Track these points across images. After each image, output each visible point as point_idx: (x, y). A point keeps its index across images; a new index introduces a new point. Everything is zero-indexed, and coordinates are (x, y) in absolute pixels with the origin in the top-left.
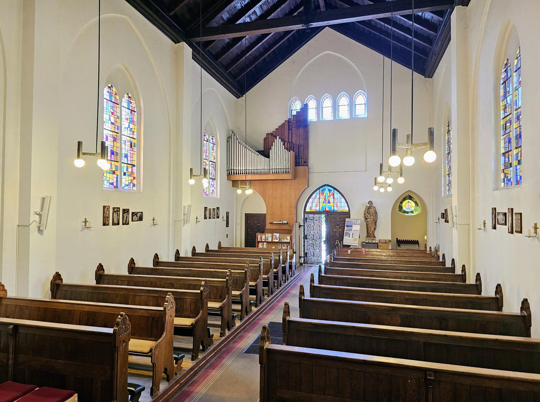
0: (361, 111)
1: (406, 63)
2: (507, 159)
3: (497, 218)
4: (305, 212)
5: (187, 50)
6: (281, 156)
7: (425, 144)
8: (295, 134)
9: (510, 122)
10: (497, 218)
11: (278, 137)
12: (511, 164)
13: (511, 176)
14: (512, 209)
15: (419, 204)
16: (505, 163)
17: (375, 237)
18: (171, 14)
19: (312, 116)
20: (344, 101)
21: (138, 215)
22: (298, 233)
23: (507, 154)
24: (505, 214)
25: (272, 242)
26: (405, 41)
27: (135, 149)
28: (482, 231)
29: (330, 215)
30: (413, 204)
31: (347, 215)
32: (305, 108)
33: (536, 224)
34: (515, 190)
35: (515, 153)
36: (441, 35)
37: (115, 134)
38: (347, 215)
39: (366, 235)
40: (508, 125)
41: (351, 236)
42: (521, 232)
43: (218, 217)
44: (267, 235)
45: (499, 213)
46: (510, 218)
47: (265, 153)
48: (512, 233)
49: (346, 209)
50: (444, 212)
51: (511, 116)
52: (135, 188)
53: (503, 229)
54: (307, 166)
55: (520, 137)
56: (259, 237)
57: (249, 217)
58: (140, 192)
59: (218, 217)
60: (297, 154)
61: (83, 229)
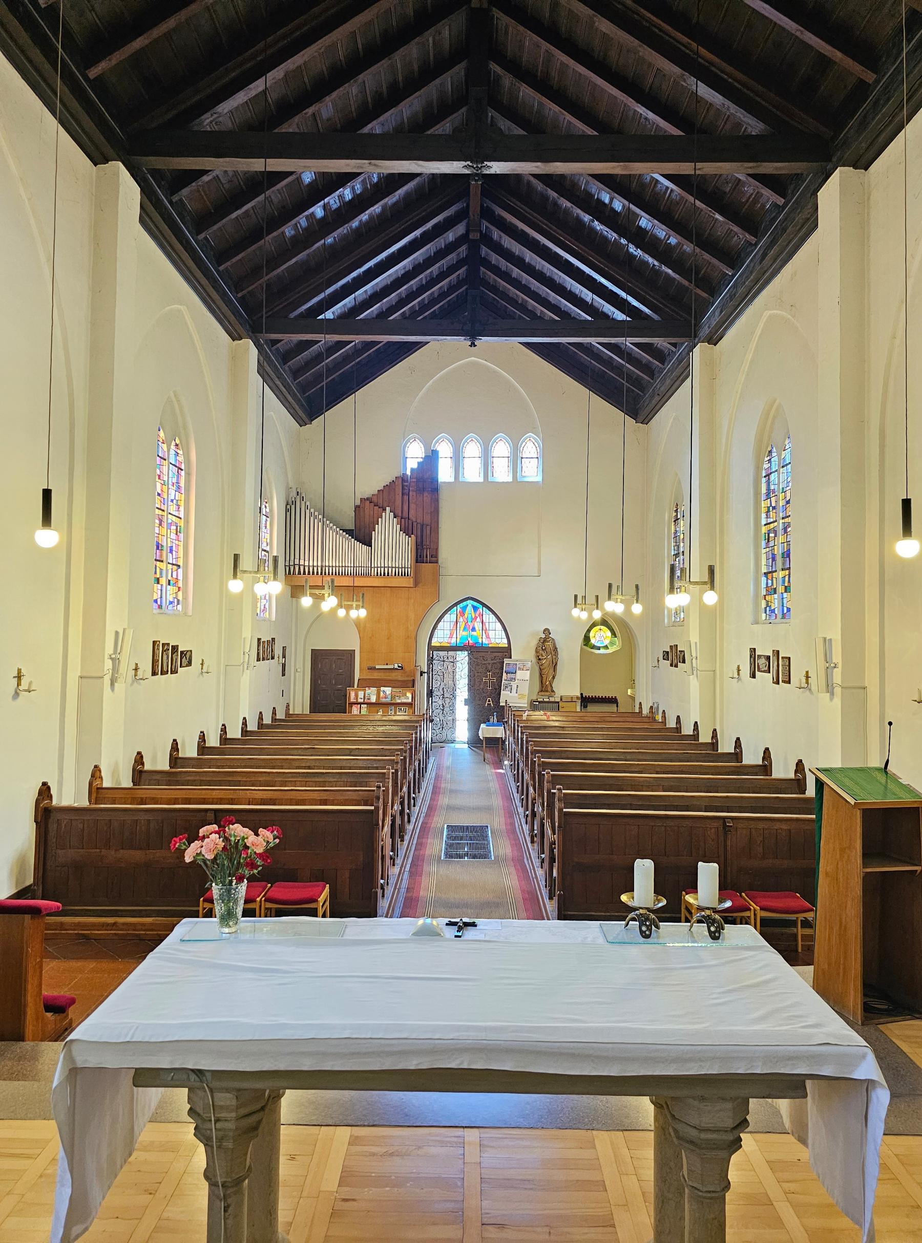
0: (532, 471)
1: (618, 404)
2: (770, 582)
3: (758, 663)
4: (431, 648)
5: (250, 351)
6: (392, 543)
7: (705, 583)
8: (415, 503)
9: (775, 532)
10: (758, 663)
11: (388, 509)
12: (775, 589)
13: (775, 605)
14: (778, 652)
15: (618, 634)
16: (767, 586)
17: (553, 691)
18: (240, 295)
19: (445, 474)
20: (501, 449)
21: (188, 656)
22: (422, 685)
23: (769, 575)
24: (768, 658)
25: (378, 704)
26: (618, 369)
27: (181, 536)
28: (736, 680)
29: (476, 651)
30: (609, 633)
31: (506, 652)
32: (431, 458)
33: (807, 672)
34: (782, 628)
35: (781, 576)
36: (671, 371)
37: (160, 512)
38: (506, 652)
39: (537, 687)
40: (772, 535)
41: (514, 690)
42: (789, 682)
43: (273, 658)
44: (368, 691)
45: (759, 656)
46: (776, 663)
47: (361, 534)
48: (778, 683)
49: (504, 643)
50: (668, 650)
51: (776, 524)
52: (180, 607)
53: (765, 678)
54: (437, 562)
55: (788, 556)
56: (353, 694)
57: (318, 656)
58: (185, 614)
59: (273, 658)
60: (419, 540)
61: (133, 682)
